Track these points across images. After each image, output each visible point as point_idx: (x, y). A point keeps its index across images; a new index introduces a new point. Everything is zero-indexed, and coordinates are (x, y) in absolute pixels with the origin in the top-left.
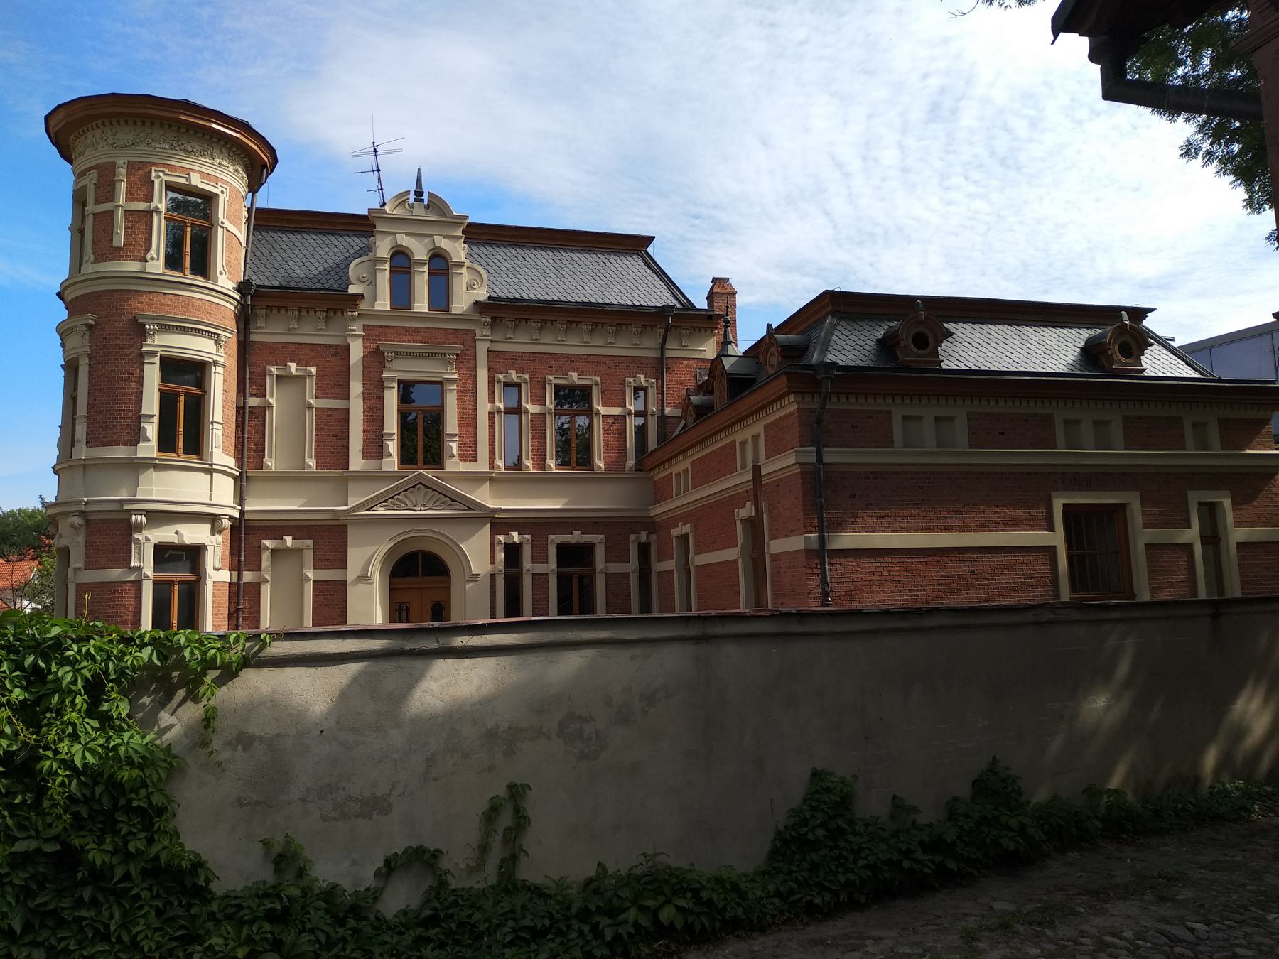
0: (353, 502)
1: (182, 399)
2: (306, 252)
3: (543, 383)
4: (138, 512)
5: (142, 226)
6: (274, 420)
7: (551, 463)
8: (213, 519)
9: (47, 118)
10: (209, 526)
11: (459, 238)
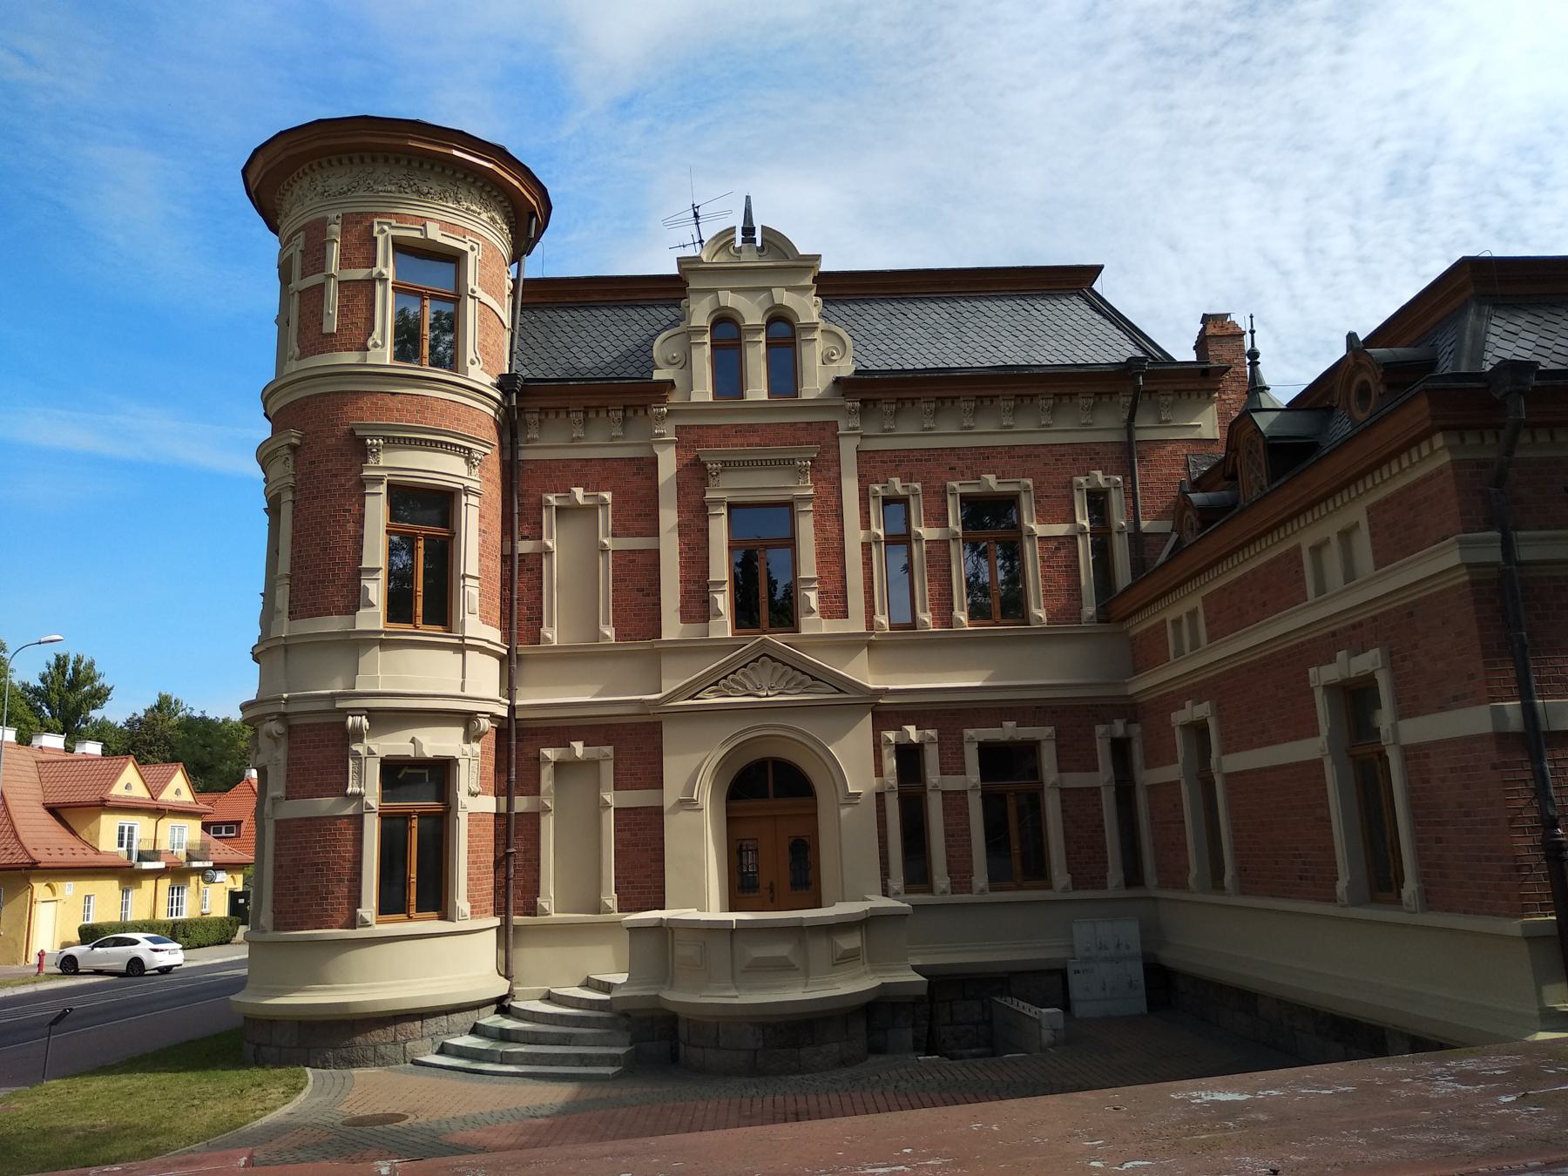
0: (668, 686)
2: (595, 334)
3: (943, 493)
4: (356, 712)
5: (361, 301)
6: (555, 570)
7: (962, 616)
8: (466, 719)
9: (245, 172)
10: (460, 731)
11: (807, 289)
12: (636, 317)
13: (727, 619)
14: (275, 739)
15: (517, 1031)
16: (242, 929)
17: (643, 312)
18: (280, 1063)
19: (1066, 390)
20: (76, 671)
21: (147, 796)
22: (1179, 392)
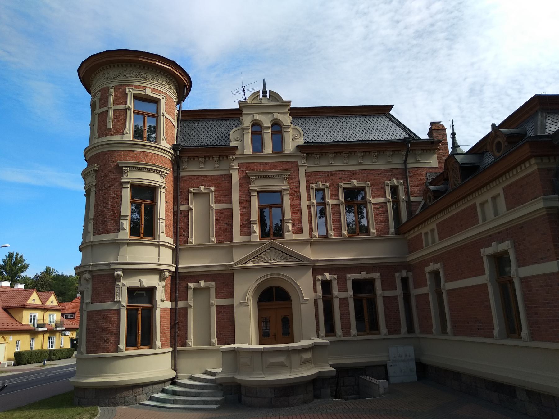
1: (143, 207)
2: (208, 130)
3: (337, 187)
4: (118, 270)
6: (194, 218)
7: (345, 232)
8: (160, 272)
9: (78, 70)
10: (157, 277)
11: (286, 113)
12: (223, 124)
13: (258, 234)
14: (87, 280)
15: (179, 392)
16: (75, 353)
17: (226, 122)
18: (88, 405)
19: (382, 149)
20: (16, 258)
21: (41, 303)
22: (423, 150)
